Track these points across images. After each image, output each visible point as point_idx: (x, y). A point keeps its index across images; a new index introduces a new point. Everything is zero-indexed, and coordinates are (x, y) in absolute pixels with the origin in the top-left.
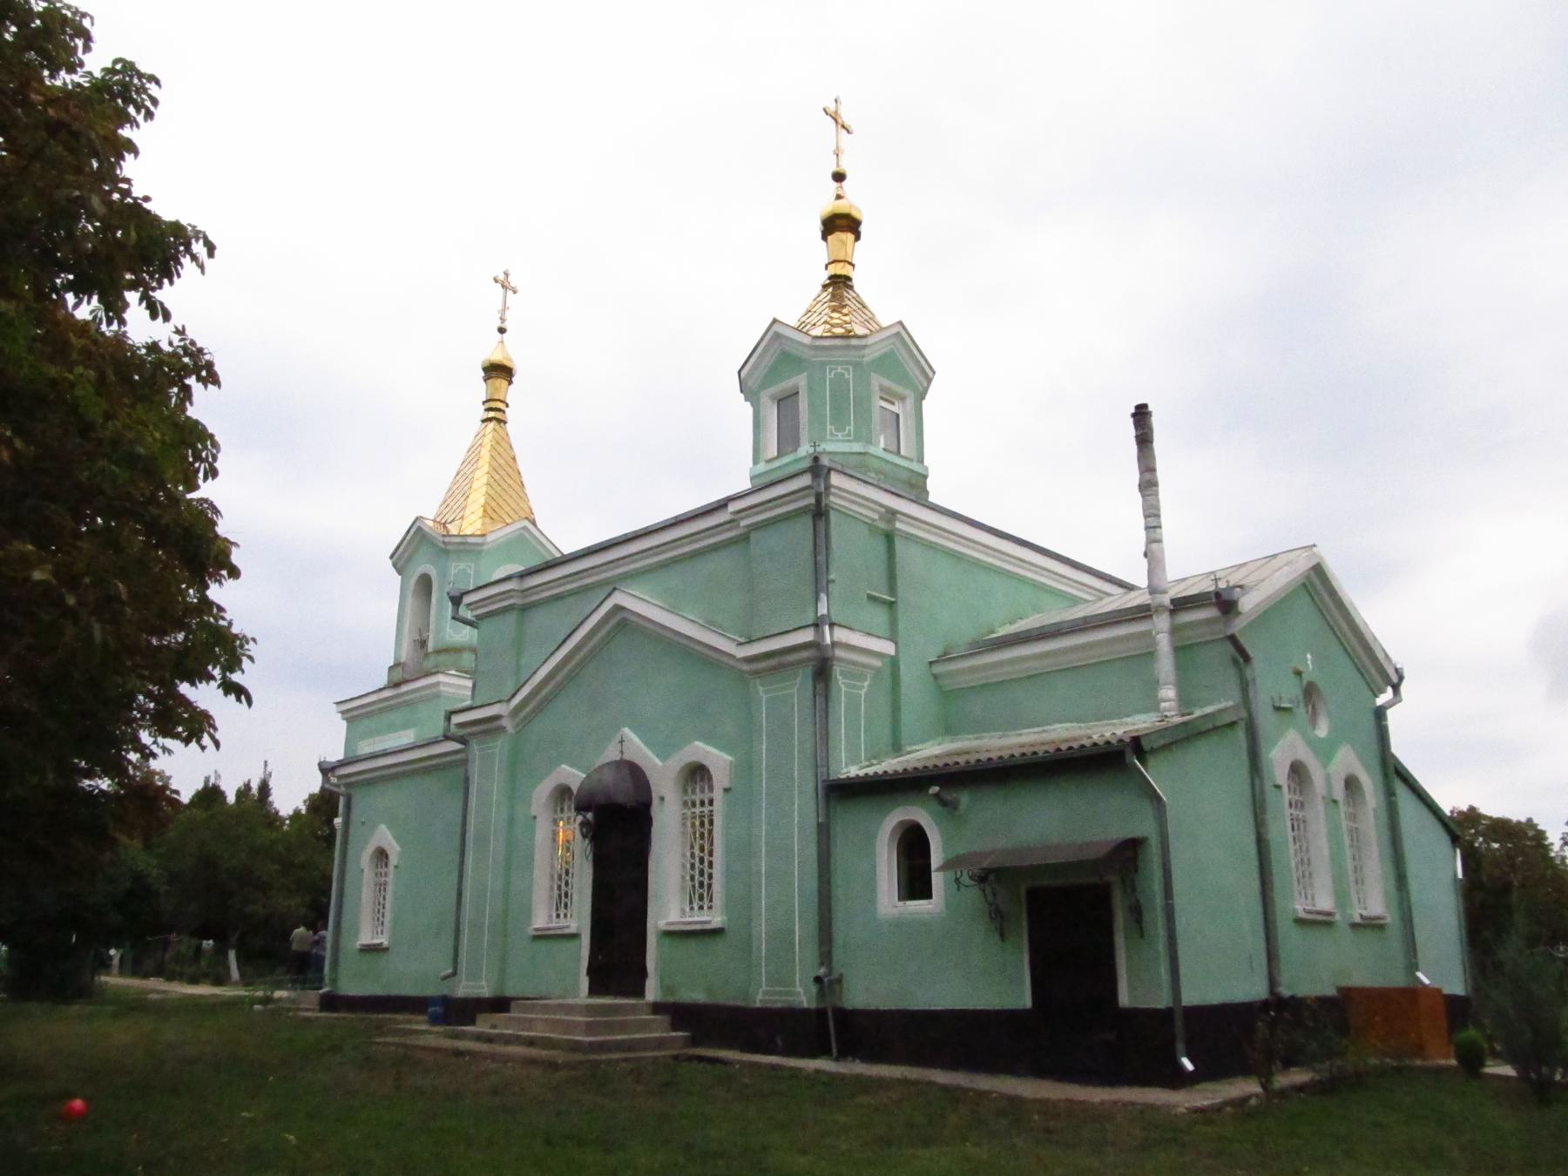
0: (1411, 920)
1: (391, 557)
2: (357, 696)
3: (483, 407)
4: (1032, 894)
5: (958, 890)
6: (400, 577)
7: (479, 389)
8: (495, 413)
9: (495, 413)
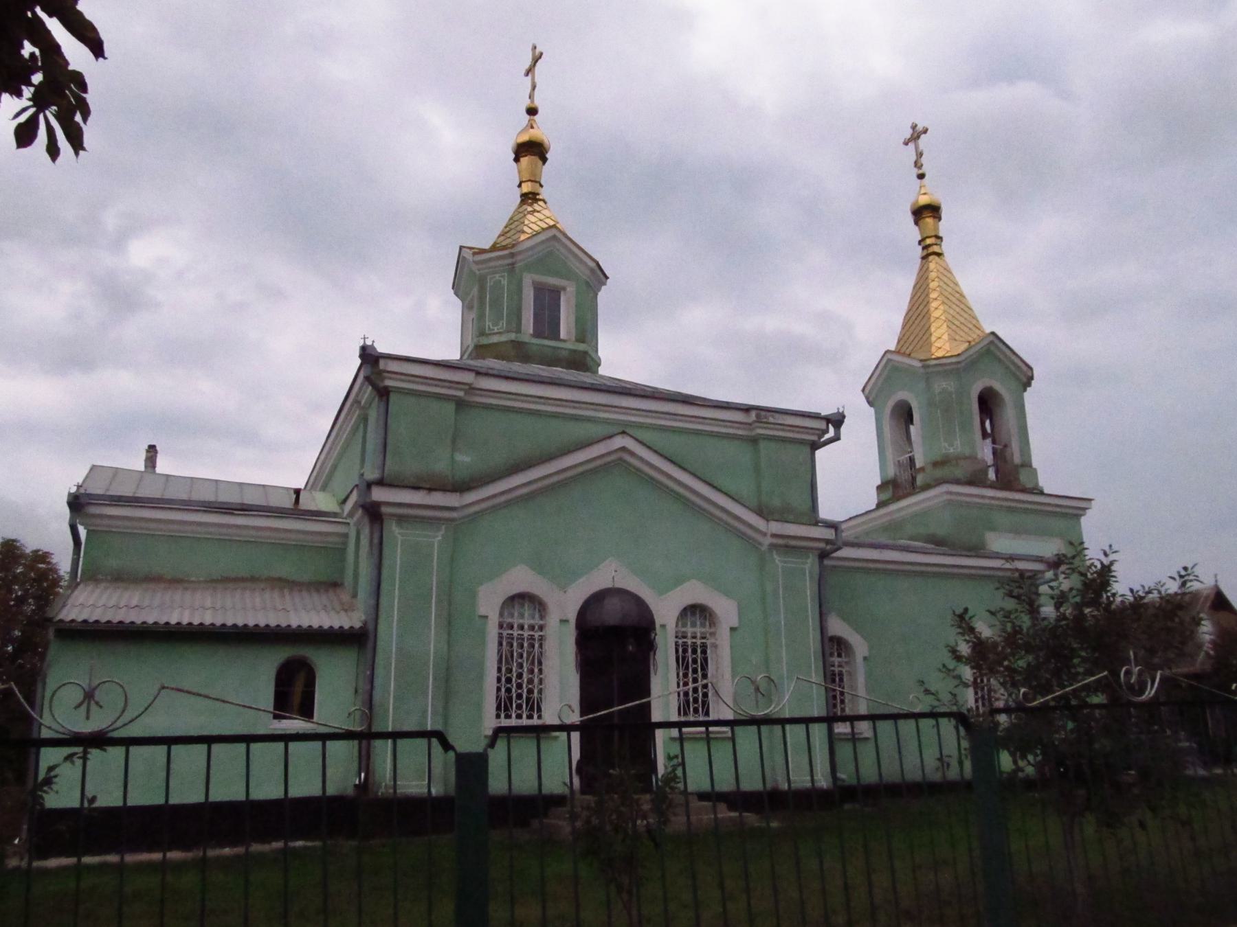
0: (854, 559)
1: (863, 390)
2: (863, 512)
3: (920, 248)
4: (521, 332)
5: (906, 143)
6: (872, 408)
7: (913, 233)
8: (930, 249)
9: (930, 249)
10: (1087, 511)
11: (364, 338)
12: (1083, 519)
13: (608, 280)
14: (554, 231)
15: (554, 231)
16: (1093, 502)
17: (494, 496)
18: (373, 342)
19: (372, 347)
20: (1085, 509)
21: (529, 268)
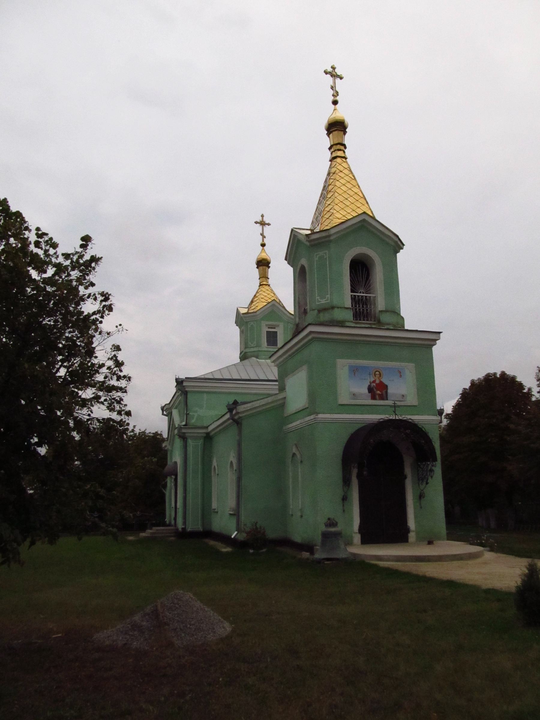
10: (437, 342)
11: (176, 376)
12: (434, 348)
13: (404, 246)
14: (274, 302)
15: (274, 302)
16: (441, 334)
17: (193, 433)
18: (179, 376)
19: (179, 378)
20: (435, 340)
21: (262, 319)
